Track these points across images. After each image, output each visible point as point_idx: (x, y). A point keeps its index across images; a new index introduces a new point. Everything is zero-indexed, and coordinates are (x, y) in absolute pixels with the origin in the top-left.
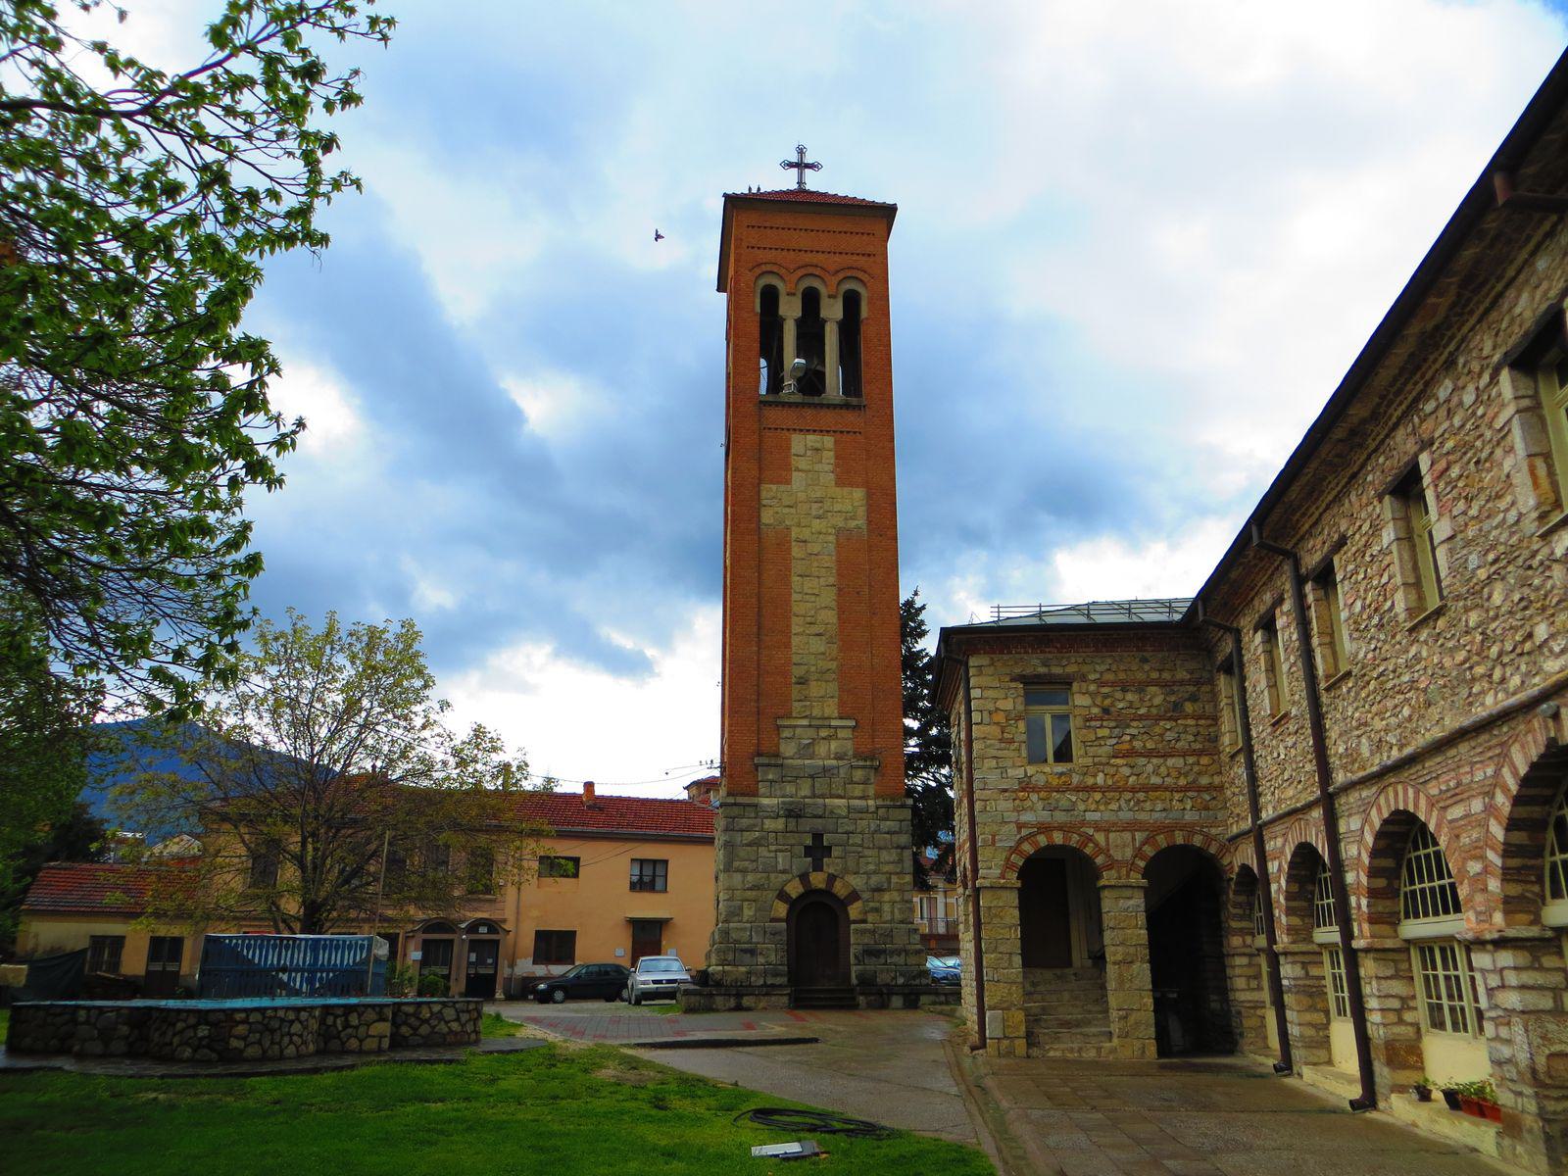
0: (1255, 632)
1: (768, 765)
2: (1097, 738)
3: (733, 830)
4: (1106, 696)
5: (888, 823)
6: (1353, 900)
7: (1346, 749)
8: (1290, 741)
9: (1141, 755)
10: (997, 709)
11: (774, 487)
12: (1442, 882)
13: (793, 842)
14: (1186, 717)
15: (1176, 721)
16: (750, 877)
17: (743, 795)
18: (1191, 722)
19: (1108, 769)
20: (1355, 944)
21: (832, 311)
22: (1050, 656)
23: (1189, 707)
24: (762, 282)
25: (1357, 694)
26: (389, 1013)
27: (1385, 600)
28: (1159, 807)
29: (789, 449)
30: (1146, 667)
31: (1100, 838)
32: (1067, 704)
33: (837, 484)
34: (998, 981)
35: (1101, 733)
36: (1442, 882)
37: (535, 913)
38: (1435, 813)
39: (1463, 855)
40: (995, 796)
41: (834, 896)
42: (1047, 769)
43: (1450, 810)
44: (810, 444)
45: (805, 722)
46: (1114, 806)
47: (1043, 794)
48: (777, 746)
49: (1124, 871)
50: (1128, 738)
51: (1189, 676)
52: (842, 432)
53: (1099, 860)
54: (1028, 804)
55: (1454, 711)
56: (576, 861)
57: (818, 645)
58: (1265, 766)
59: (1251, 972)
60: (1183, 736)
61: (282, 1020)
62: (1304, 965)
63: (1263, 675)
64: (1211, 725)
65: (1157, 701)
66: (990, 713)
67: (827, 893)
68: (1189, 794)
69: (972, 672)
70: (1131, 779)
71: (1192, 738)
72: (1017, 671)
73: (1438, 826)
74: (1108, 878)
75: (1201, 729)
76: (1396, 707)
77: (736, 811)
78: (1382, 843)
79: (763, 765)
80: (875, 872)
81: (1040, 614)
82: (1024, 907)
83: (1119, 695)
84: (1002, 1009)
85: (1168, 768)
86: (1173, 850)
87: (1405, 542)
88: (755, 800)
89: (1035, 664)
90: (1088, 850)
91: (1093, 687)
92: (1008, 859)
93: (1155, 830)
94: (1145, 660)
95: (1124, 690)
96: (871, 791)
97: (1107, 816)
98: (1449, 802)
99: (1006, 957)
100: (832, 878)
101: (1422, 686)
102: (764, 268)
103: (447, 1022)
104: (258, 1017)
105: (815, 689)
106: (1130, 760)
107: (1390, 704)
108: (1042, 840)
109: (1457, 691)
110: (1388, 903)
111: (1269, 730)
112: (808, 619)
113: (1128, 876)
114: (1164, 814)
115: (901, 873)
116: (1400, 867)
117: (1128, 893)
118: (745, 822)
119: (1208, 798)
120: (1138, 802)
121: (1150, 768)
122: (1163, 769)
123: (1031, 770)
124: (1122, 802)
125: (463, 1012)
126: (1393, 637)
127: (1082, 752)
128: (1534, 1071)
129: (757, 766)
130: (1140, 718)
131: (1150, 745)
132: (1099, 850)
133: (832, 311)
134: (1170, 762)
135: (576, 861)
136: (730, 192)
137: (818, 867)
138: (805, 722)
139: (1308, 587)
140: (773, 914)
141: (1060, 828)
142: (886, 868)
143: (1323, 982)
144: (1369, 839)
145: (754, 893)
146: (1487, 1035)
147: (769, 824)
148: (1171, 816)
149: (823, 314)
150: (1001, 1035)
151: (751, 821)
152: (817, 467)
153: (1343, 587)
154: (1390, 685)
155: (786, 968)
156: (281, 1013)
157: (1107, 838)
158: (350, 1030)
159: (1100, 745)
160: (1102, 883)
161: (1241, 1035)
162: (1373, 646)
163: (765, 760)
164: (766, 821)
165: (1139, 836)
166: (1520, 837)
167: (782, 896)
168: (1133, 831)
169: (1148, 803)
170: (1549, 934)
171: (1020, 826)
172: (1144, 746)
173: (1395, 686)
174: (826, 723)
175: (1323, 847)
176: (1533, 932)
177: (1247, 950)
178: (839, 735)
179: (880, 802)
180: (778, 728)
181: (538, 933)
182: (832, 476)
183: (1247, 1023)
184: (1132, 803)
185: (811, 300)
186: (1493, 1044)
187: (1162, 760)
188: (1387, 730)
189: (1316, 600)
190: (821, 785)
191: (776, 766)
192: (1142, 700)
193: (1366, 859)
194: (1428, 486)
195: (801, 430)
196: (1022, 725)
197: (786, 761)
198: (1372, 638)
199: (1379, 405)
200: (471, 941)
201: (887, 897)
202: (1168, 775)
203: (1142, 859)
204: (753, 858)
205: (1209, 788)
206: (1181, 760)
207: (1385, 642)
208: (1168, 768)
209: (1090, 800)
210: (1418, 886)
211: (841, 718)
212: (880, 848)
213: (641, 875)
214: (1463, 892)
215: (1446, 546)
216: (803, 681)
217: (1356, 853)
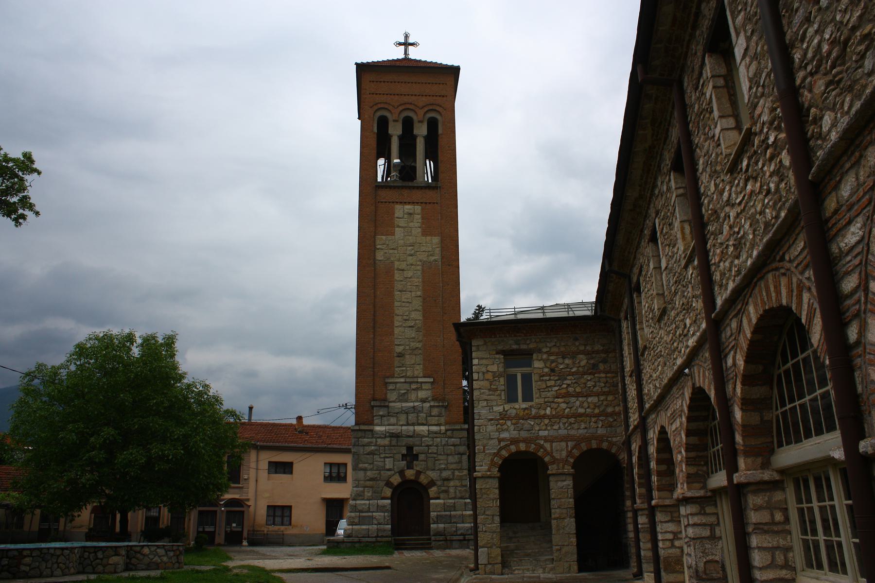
2: (547, 387)
4: (553, 361)
9: (573, 396)
11: (384, 237)
14: (599, 373)
16: (369, 473)
17: (364, 424)
18: (603, 375)
19: (553, 405)
21: (421, 130)
23: (601, 367)
24: (379, 114)
26: (123, 552)
28: (583, 426)
30: (577, 344)
31: (547, 446)
35: (549, 383)
37: (267, 495)
41: (420, 484)
42: (517, 406)
45: (402, 380)
46: (556, 427)
47: (514, 421)
48: (386, 394)
50: (565, 386)
53: (547, 459)
54: (505, 427)
56: (291, 464)
57: (412, 333)
61: (52, 555)
65: (583, 363)
66: (484, 373)
67: (416, 482)
69: (474, 349)
71: (603, 385)
72: (500, 347)
74: (552, 469)
77: (360, 434)
80: (444, 469)
82: (502, 488)
83: (560, 360)
88: (370, 427)
89: (511, 344)
90: (540, 454)
91: (545, 356)
92: (492, 460)
93: (579, 441)
94: (576, 339)
95: (564, 358)
96: (442, 420)
97: (552, 433)
100: (419, 473)
103: (159, 557)
104: (38, 553)
105: (409, 360)
106: (567, 399)
108: (513, 448)
110: (668, 478)
113: (563, 468)
115: (461, 469)
117: (564, 478)
120: (571, 424)
121: (578, 403)
122: (585, 405)
123: (507, 407)
124: (561, 424)
128: (697, 571)
129: (373, 407)
130: (573, 374)
131: (578, 390)
132: (547, 453)
133: (421, 130)
134: (590, 399)
135: (291, 464)
137: (410, 467)
138: (402, 380)
141: (525, 440)
149: (415, 132)
150: (486, 562)
151: (369, 440)
155: (390, 526)
156: (52, 551)
157: (551, 446)
158: (98, 561)
160: (549, 472)
163: (378, 403)
166: (694, 440)
167: (388, 484)
168: (567, 441)
170: (709, 494)
171: (500, 441)
174: (415, 380)
176: (701, 493)
179: (448, 427)
181: (269, 507)
185: (408, 124)
191: (385, 406)
192: (574, 363)
197: (391, 404)
201: (452, 483)
202: (588, 407)
211: (424, 377)
213: (331, 472)
216: (401, 355)
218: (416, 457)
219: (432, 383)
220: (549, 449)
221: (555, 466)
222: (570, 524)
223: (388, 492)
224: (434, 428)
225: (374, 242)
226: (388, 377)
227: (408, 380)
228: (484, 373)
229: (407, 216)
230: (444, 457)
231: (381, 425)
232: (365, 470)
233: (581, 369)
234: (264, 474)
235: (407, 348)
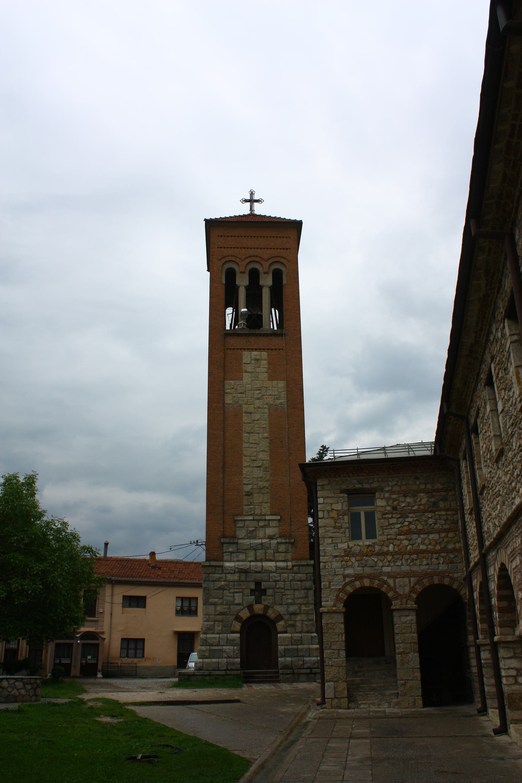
1: (229, 543)
2: (389, 524)
3: (209, 581)
4: (394, 500)
5: (299, 575)
9: (415, 533)
10: (333, 510)
11: (232, 382)
13: (244, 587)
15: (434, 512)
16: (219, 608)
17: (214, 560)
18: (443, 513)
19: (397, 542)
21: (266, 281)
22: (363, 478)
23: (442, 504)
24: (227, 266)
28: (425, 562)
29: (241, 360)
30: (418, 482)
31: (391, 581)
32: (373, 505)
33: (269, 379)
34: (332, 666)
35: (392, 521)
40: (331, 560)
41: (268, 618)
42: (361, 543)
44: (253, 357)
45: (251, 518)
46: (399, 563)
47: (358, 558)
48: (235, 531)
49: (404, 600)
51: (442, 487)
52: (272, 349)
53: (390, 595)
54: (350, 563)
56: (144, 598)
57: (259, 473)
60: (438, 521)
64: (453, 515)
65: (424, 501)
66: (328, 511)
67: (263, 616)
68: (442, 554)
69: (319, 488)
70: (409, 547)
71: (443, 522)
72: (344, 487)
74: (396, 604)
75: (448, 517)
77: (211, 570)
79: (226, 543)
80: (292, 604)
81: (358, 454)
83: (402, 499)
84: (334, 682)
85: (430, 540)
88: (220, 563)
89: (354, 483)
90: (383, 589)
91: (387, 495)
92: (338, 596)
94: (417, 478)
96: (289, 556)
97: (395, 569)
99: (336, 652)
100: (267, 608)
102: (227, 259)
103: (18, 690)
105: (257, 498)
106: (409, 537)
108: (358, 584)
113: (406, 603)
114: (427, 567)
115: (307, 604)
117: (407, 613)
118: (217, 576)
119: (453, 556)
120: (413, 560)
121: (419, 540)
122: (427, 541)
123: (351, 544)
124: (404, 561)
125: (27, 684)
127: (381, 533)
129: (223, 544)
130: (414, 512)
131: (420, 527)
132: (390, 589)
133: (266, 281)
134: (431, 536)
136: (208, 218)
138: (251, 518)
140: (233, 629)
145: (221, 617)
147: (230, 577)
148: (431, 567)
149: (261, 283)
150: (333, 697)
151: (219, 576)
159: (391, 528)
160: (393, 607)
163: (227, 540)
167: (238, 618)
168: (409, 577)
169: (418, 561)
171: (345, 577)
172: (416, 528)
174: (263, 518)
178: (271, 525)
179: (294, 563)
182: (266, 375)
184: (409, 561)
185: (254, 275)
187: (426, 536)
190: (260, 553)
191: (234, 543)
192: (415, 501)
195: (248, 349)
196: (346, 518)
197: (240, 541)
200: (83, 644)
201: (299, 618)
202: (430, 544)
203: (414, 593)
204: (221, 597)
206: (437, 535)
208: (430, 540)
209: (385, 560)
211: (272, 515)
212: (294, 590)
213: (182, 606)
216: (249, 494)
219: (279, 520)
220: (392, 584)
221: (398, 602)
223: (237, 626)
224: (281, 564)
226: (237, 515)
228: (328, 511)
229: (254, 362)
231: (230, 561)
232: (215, 604)
234: (118, 608)
235: (255, 487)
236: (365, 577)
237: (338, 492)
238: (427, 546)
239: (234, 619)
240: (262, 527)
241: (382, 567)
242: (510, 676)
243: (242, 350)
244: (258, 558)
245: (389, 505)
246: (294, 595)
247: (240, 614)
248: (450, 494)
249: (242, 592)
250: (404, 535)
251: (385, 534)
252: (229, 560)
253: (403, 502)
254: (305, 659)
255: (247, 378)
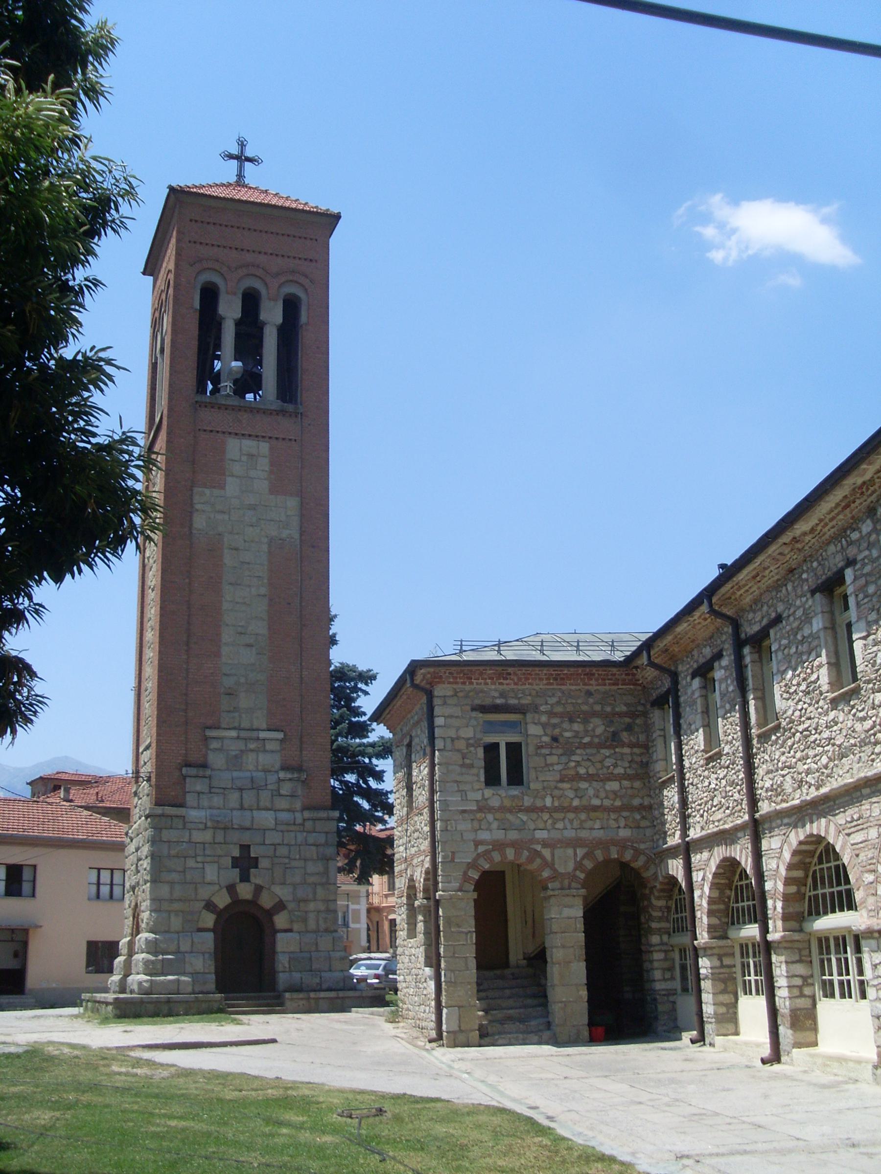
0: (693, 678)
2: (547, 765)
4: (554, 726)
6: (770, 903)
7: (772, 785)
8: (722, 773)
9: (585, 780)
10: (458, 738)
11: (207, 491)
12: (839, 888)
15: (614, 749)
18: (626, 750)
19: (556, 793)
20: (770, 937)
21: (272, 315)
23: (625, 736)
24: (205, 277)
25: (784, 742)
27: (812, 672)
30: (591, 700)
31: (547, 853)
33: (271, 492)
36: (839, 888)
38: (841, 837)
39: (861, 869)
43: (852, 836)
45: (234, 733)
46: (560, 825)
48: (205, 756)
50: (573, 764)
55: (861, 764)
58: (694, 794)
59: (666, 965)
62: (720, 957)
63: (699, 716)
65: (599, 730)
66: (453, 740)
71: (627, 765)
73: (843, 847)
76: (815, 756)
78: (797, 859)
83: (566, 725)
86: (607, 862)
87: (830, 631)
92: (465, 873)
97: (555, 835)
98: (853, 830)
100: (259, 889)
101: (838, 743)
105: (244, 701)
107: (811, 753)
109: (863, 749)
111: (702, 762)
112: (239, 629)
116: (807, 876)
120: (582, 822)
121: (591, 792)
124: (566, 821)
126: (817, 702)
130: (585, 746)
131: (592, 771)
132: (546, 864)
133: (272, 315)
139: (746, 650)
140: (201, 925)
142: (311, 879)
143: (734, 970)
144: (787, 856)
146: (871, 998)
149: (263, 316)
152: (252, 473)
153: (776, 656)
154: (812, 738)
157: (553, 855)
161: (656, 1018)
162: (799, 707)
163: (193, 771)
164: (194, 833)
165: (580, 852)
167: (210, 906)
171: (477, 843)
173: (816, 740)
174: (243, 734)
175: (746, 861)
177: (664, 948)
180: (206, 739)
183: (660, 1008)
185: (251, 302)
186: (874, 1003)
188: (808, 772)
189: (752, 662)
192: (586, 731)
193: (783, 871)
194: (851, 594)
198: (800, 700)
199: (817, 525)
201: (312, 906)
202: (607, 797)
203: (582, 872)
205: (641, 808)
207: (810, 705)
210: (820, 891)
214: (858, 896)
215: (862, 642)
217: (775, 867)
218: (255, 863)
219: (282, 741)
222: (579, 970)
223: (209, 920)
224: (284, 816)
225: (191, 497)
226: (210, 728)
227: (243, 734)
228: (453, 740)
229: (247, 459)
230: (301, 864)
231: (198, 807)
232: (172, 883)
233: (596, 740)
235: (242, 680)
236: (508, 845)
237: (469, 708)
238: (602, 800)
239: (204, 908)
240: (252, 751)
241: (535, 830)
242: (794, 986)
243: (226, 435)
244: (246, 806)
245: (546, 735)
246: (305, 868)
247: (212, 899)
248: (638, 721)
249: (218, 862)
250: (567, 782)
251: (540, 779)
252: (196, 805)
253: (567, 731)
254: (323, 974)
255: (232, 486)
